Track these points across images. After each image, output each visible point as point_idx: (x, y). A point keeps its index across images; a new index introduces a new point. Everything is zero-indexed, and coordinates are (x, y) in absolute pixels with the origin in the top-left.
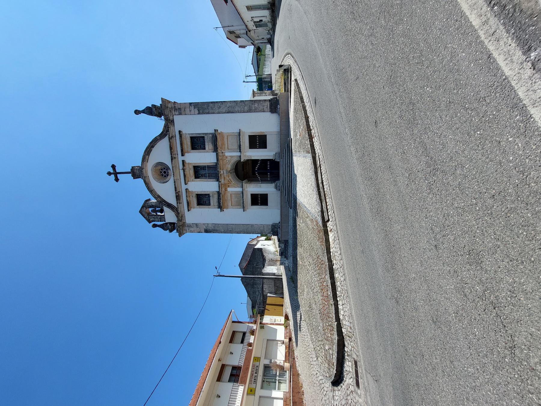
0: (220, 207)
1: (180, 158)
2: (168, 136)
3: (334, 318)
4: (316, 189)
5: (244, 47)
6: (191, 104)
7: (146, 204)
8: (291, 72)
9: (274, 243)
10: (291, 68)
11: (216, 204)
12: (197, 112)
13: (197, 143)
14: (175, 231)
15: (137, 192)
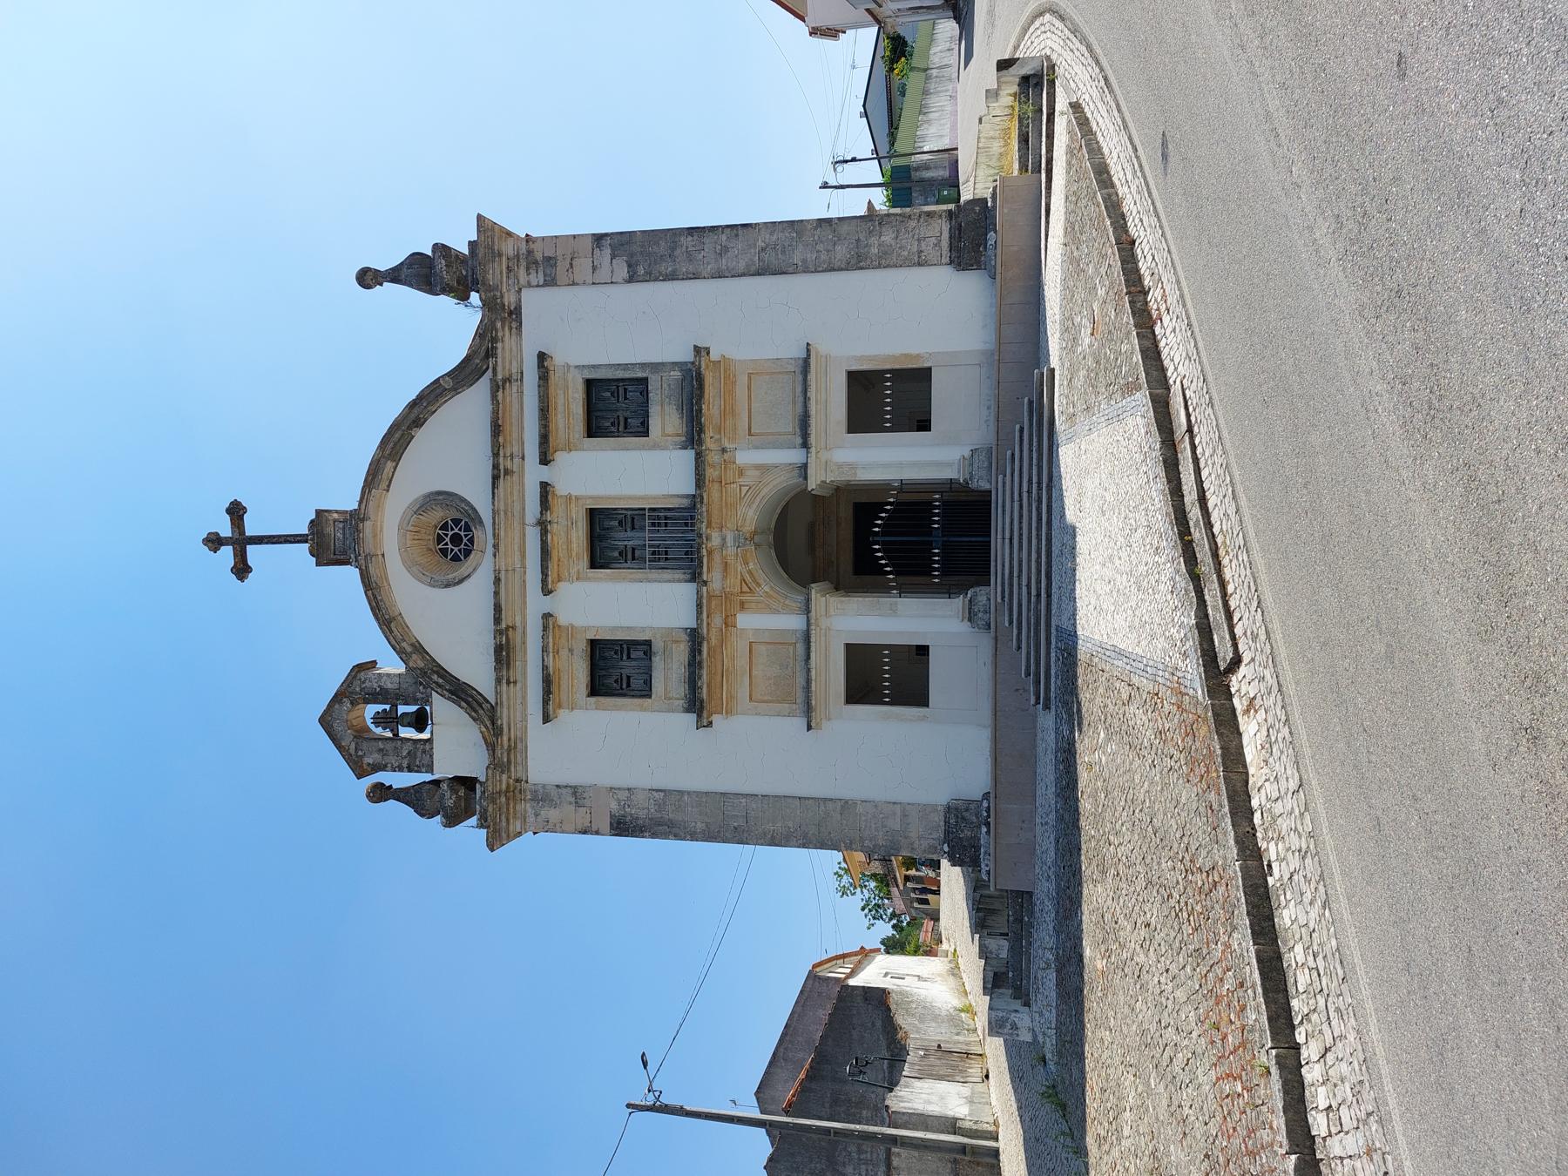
0: (696, 705)
1: (533, 473)
2: (489, 373)
3: (1282, 1137)
4: (1173, 533)
5: (832, 33)
6: (599, 239)
7: (358, 685)
8: (1052, 83)
9: (955, 971)
10: (1052, 67)
11: (679, 690)
12: (622, 271)
13: (614, 406)
14: (473, 820)
15: (325, 625)
